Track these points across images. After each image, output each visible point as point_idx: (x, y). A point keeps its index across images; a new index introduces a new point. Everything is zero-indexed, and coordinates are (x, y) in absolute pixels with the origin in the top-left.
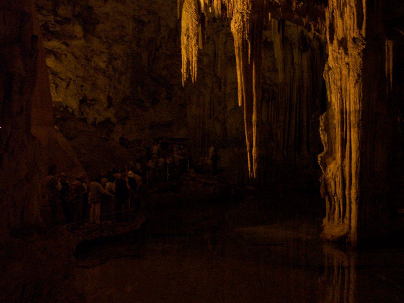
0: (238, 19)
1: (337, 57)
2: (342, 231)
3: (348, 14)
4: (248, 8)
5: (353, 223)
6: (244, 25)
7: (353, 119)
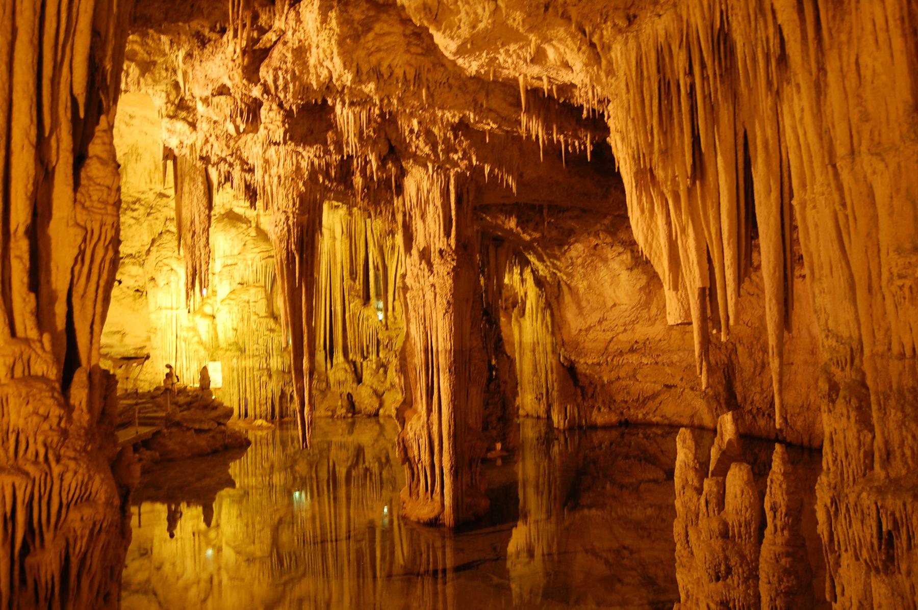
0: (281, 220)
1: (418, 275)
3: (432, 216)
4: (294, 205)
6: (289, 230)
7: (443, 361)
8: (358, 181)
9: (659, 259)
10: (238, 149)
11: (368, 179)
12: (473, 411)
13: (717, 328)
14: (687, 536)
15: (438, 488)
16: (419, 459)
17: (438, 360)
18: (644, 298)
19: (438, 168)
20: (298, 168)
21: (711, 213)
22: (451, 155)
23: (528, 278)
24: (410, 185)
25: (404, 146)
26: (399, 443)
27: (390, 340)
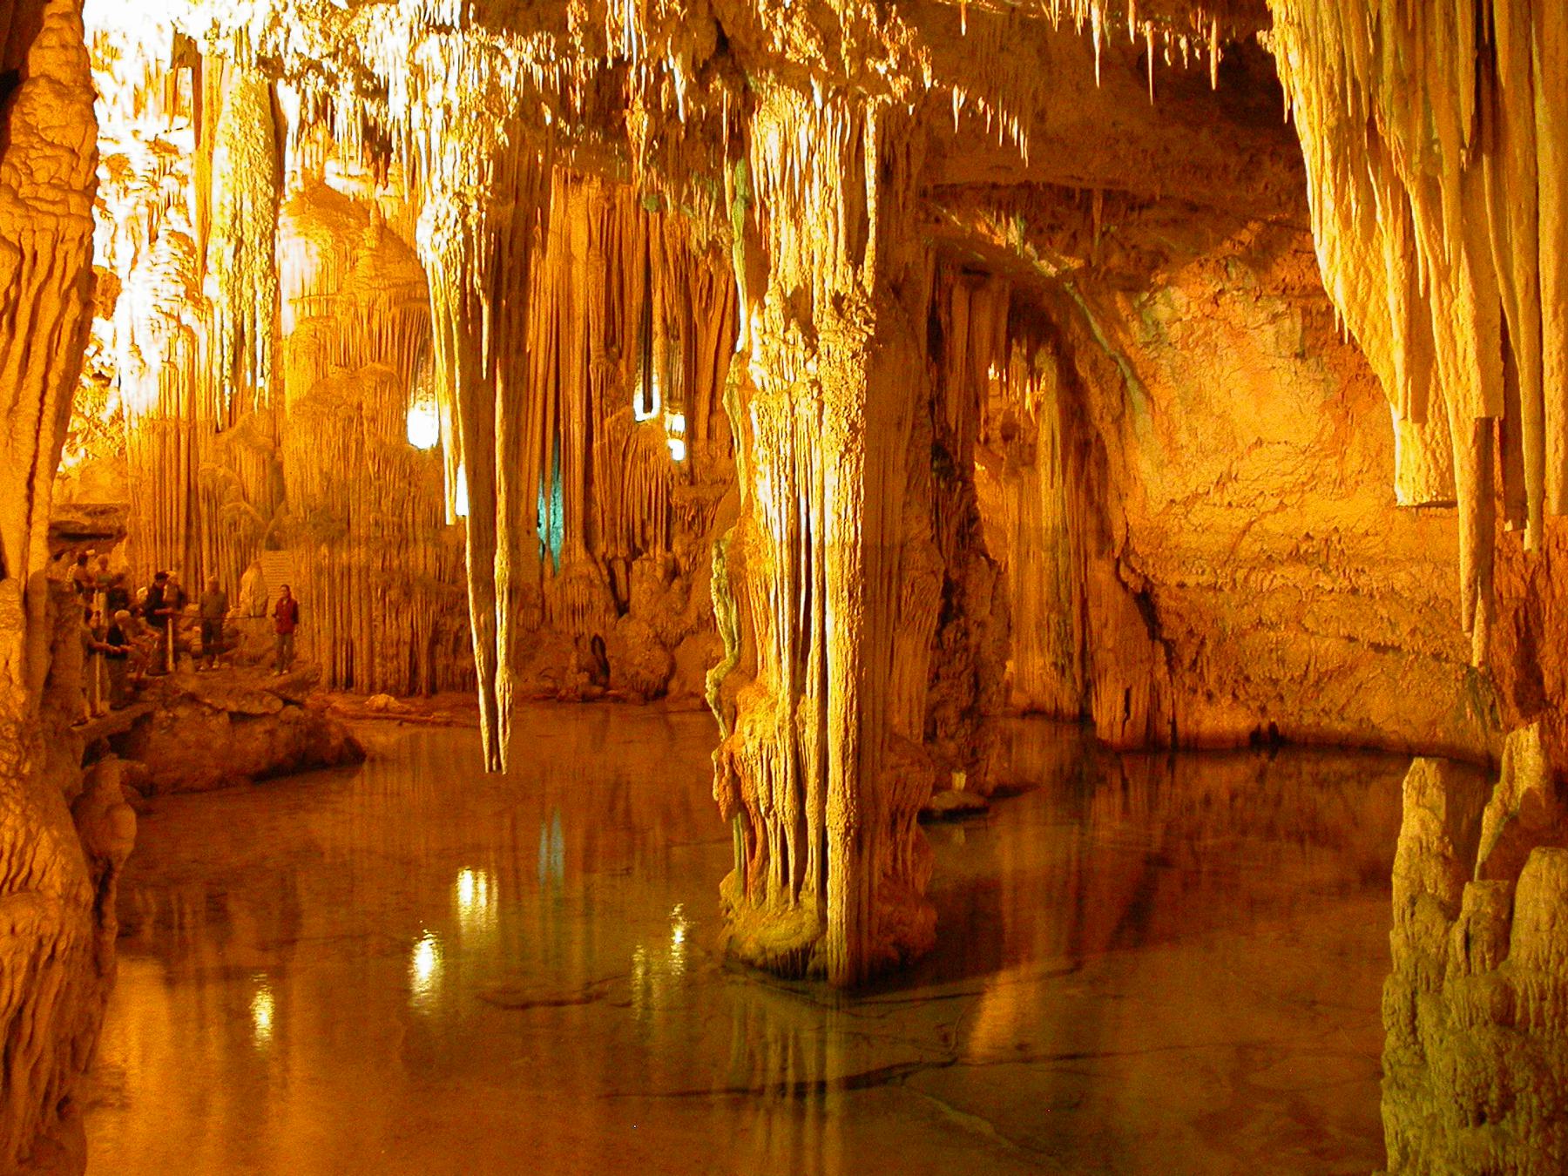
2: (796, 933)
3: (818, 210)
5: (836, 909)
6: (468, 241)
7: (835, 569)
8: (638, 121)
9: (1383, 341)
10: (351, 40)
11: (663, 118)
12: (905, 696)
13: (1514, 519)
14: (1414, 1015)
15: (811, 878)
16: (770, 807)
17: (822, 566)
18: (1331, 428)
19: (836, 94)
20: (494, 88)
21: (1516, 238)
22: (870, 63)
23: (1046, 367)
24: (765, 134)
25: (754, 38)
26: (720, 766)
27: (700, 509)
